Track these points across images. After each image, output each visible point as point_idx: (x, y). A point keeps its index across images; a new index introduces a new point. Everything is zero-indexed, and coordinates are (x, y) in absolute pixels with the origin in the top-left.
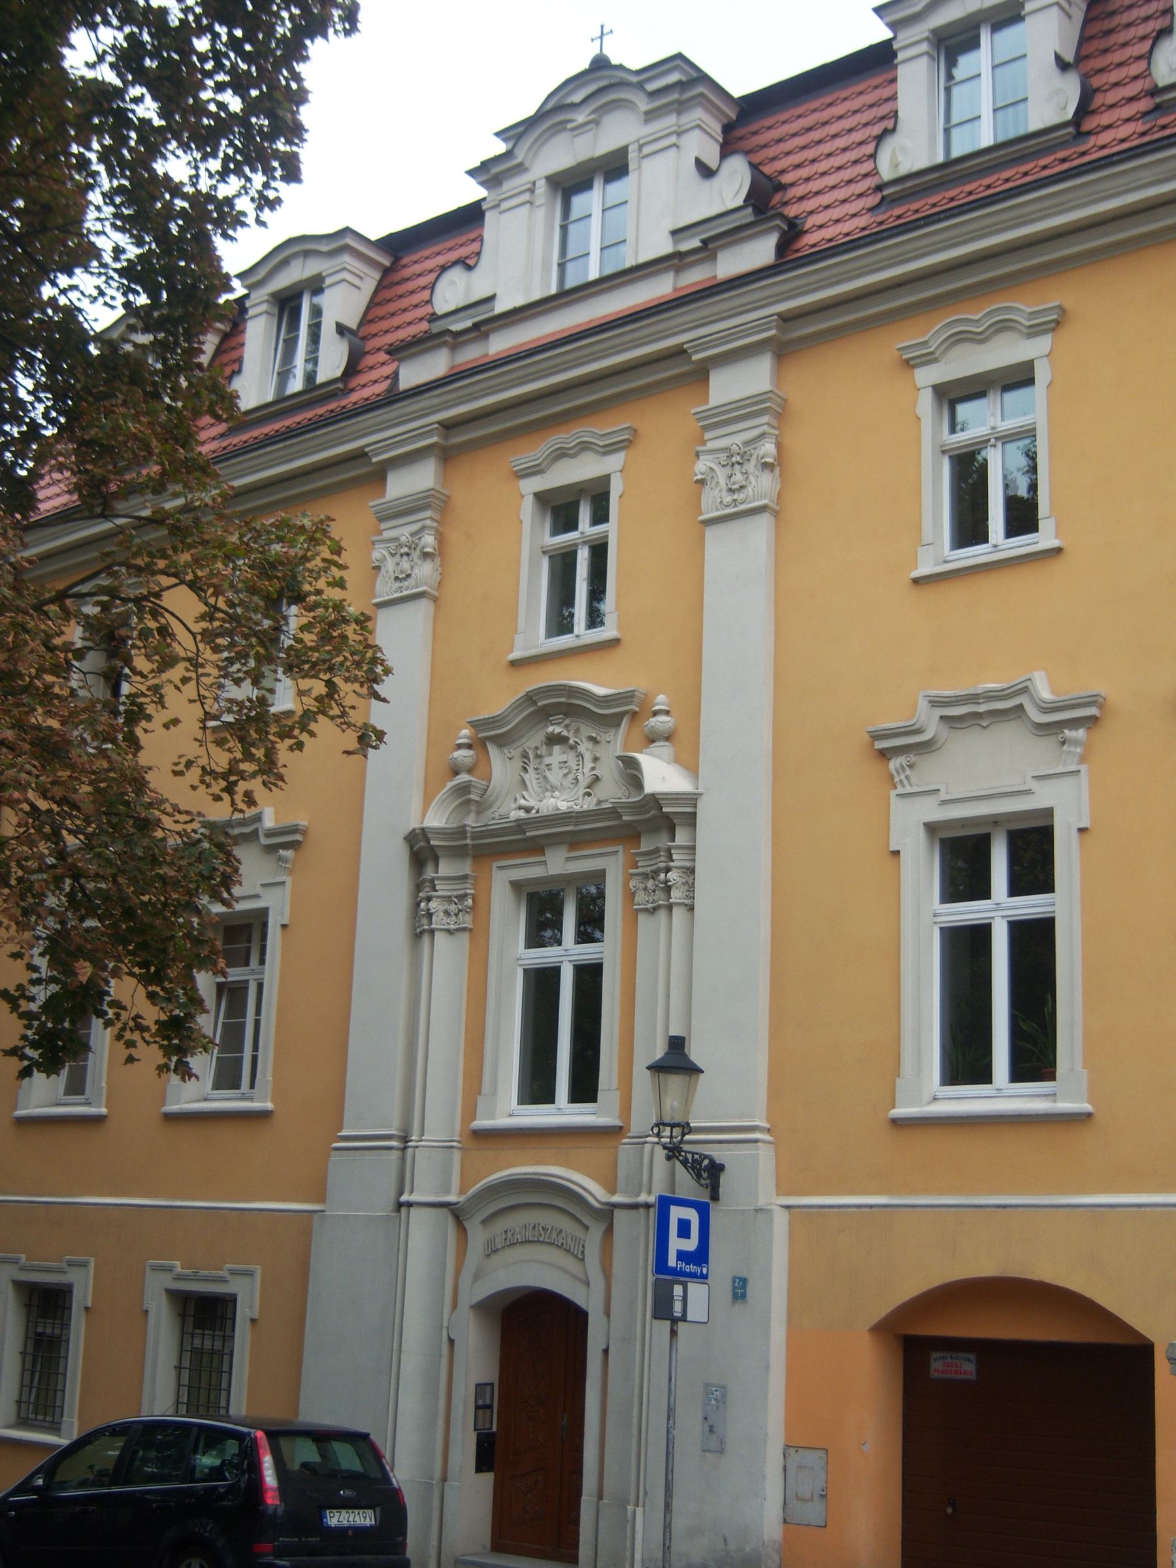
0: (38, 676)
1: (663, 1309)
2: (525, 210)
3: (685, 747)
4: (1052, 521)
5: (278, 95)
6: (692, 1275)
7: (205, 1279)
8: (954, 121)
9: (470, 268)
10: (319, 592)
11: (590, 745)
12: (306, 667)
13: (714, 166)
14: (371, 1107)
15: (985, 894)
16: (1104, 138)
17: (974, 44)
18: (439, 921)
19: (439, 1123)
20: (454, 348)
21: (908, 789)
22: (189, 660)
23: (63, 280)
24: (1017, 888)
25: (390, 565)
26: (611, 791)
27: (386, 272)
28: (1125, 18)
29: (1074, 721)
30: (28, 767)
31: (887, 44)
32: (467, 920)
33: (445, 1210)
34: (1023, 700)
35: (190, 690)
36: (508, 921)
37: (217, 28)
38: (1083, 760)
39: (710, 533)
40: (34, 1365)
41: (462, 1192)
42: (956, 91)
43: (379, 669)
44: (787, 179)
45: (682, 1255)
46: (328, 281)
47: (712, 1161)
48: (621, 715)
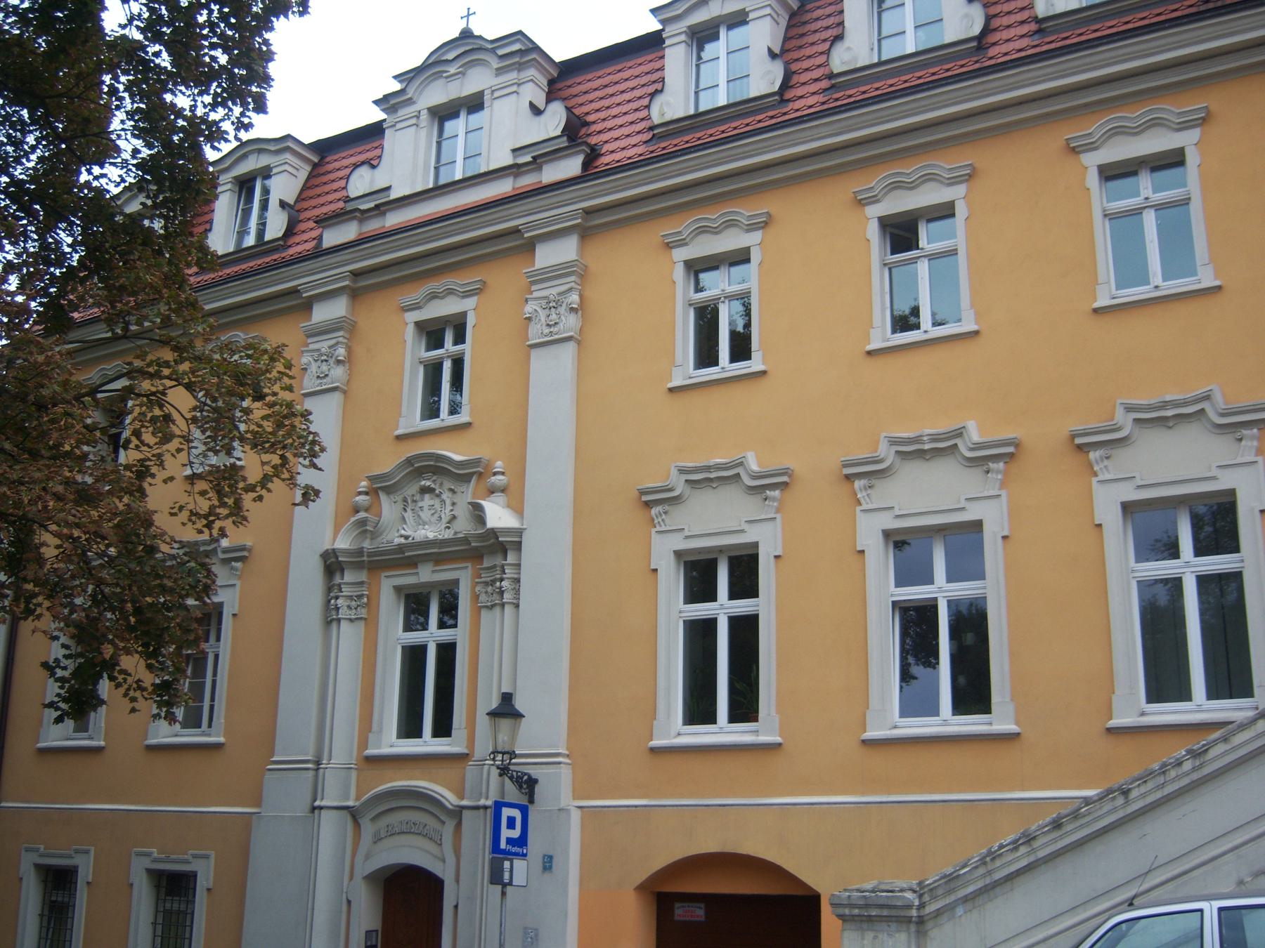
0: (78, 447)
1: (496, 877)
3: (516, 500)
5: (254, 55)
6: (516, 854)
8: (702, 87)
9: (374, 167)
10: (275, 394)
11: (450, 494)
12: (267, 445)
13: (541, 107)
14: (294, 740)
16: (798, 104)
17: (715, 37)
18: (344, 613)
19: (342, 751)
20: (361, 221)
21: (663, 528)
22: (183, 437)
23: (96, 170)
24: (733, 595)
25: (314, 367)
26: (464, 526)
27: (315, 166)
28: (813, 26)
29: (771, 485)
30: (73, 512)
32: (363, 613)
33: (344, 812)
34: (739, 470)
35: (183, 457)
36: (391, 613)
37: (213, 6)
38: (778, 511)
39: (535, 353)
40: (49, 923)
41: (357, 799)
42: (703, 67)
43: (317, 448)
44: (590, 118)
47: (530, 777)
48: (472, 474)
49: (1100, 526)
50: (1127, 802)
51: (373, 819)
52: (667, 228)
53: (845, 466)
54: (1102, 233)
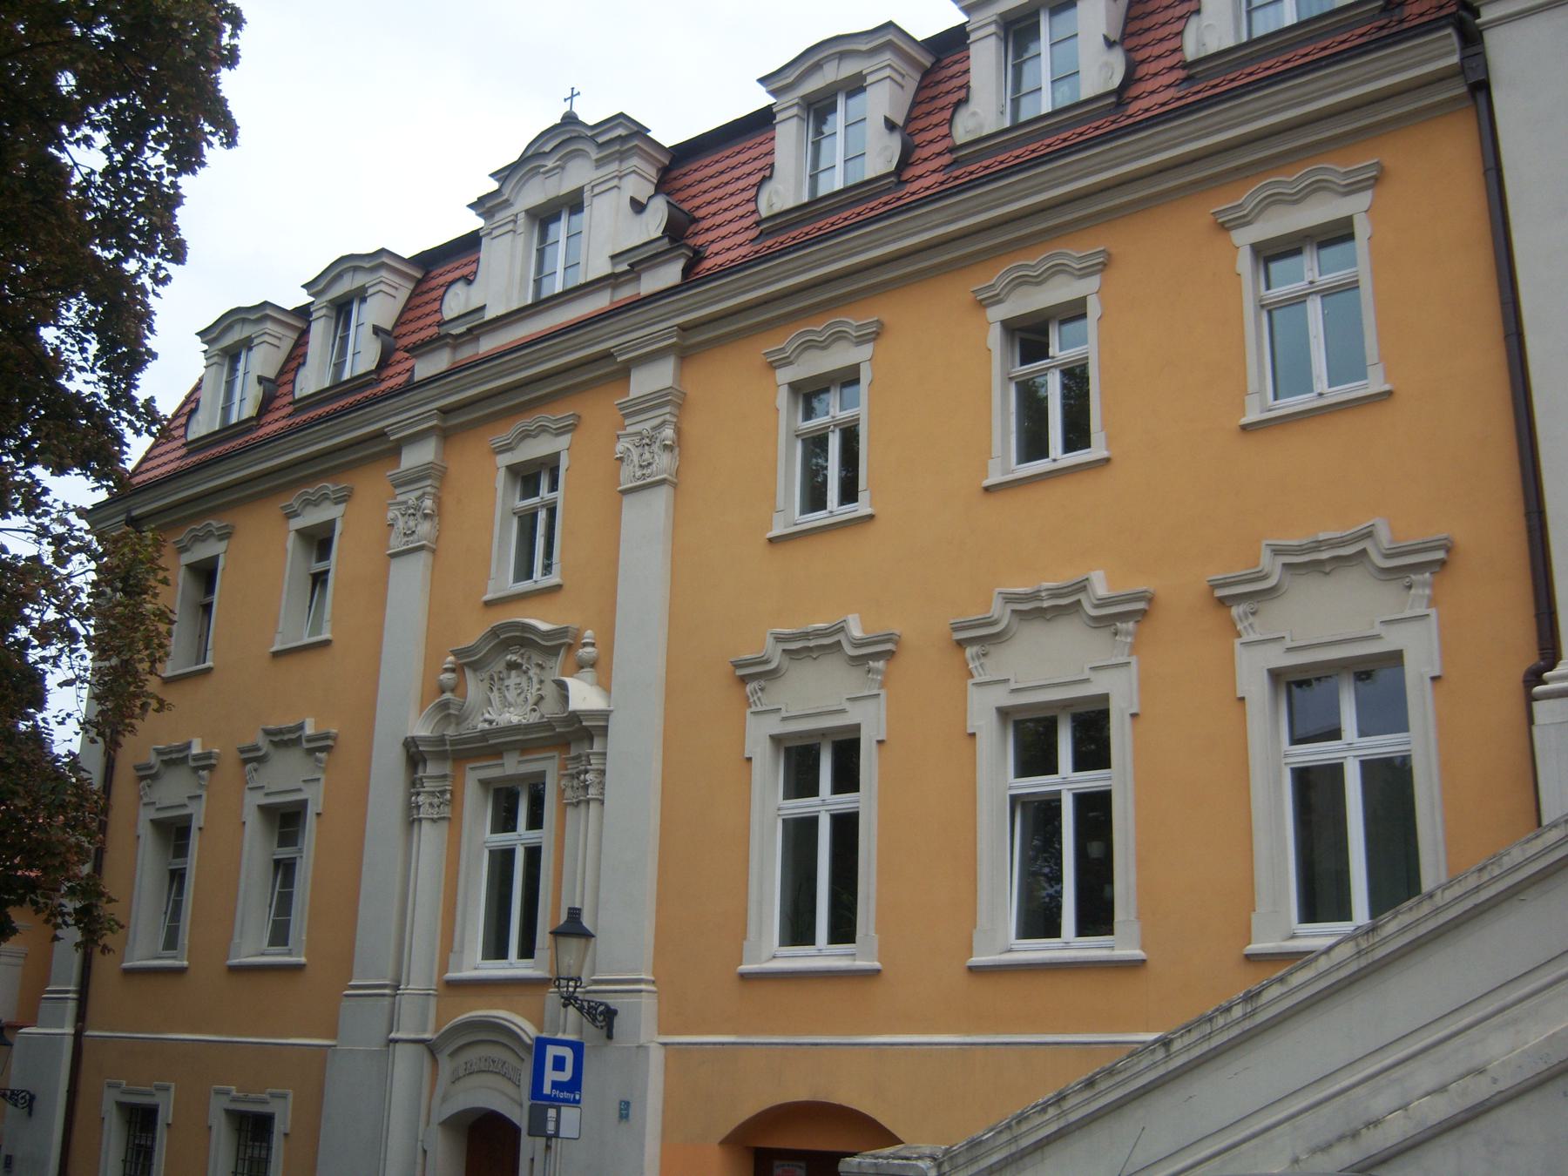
2: (509, 236)
3: (599, 669)
4: (1103, 434)
7: (254, 1101)
15: (1052, 769)
19: (420, 978)
20: (455, 348)
21: (760, 708)
25: (401, 524)
26: (550, 709)
27: (419, 282)
29: (878, 654)
31: (962, 27)
32: (446, 811)
33: (421, 1047)
34: (840, 637)
36: (477, 813)
38: (882, 685)
39: (626, 500)
41: (436, 1031)
45: (555, 1085)
46: (870, 80)
47: (607, 1006)
48: (561, 645)
49: (1242, 699)
50: (1168, 1056)
51: (453, 1054)
52: (1222, 203)
53: (956, 629)
54: (1254, 329)
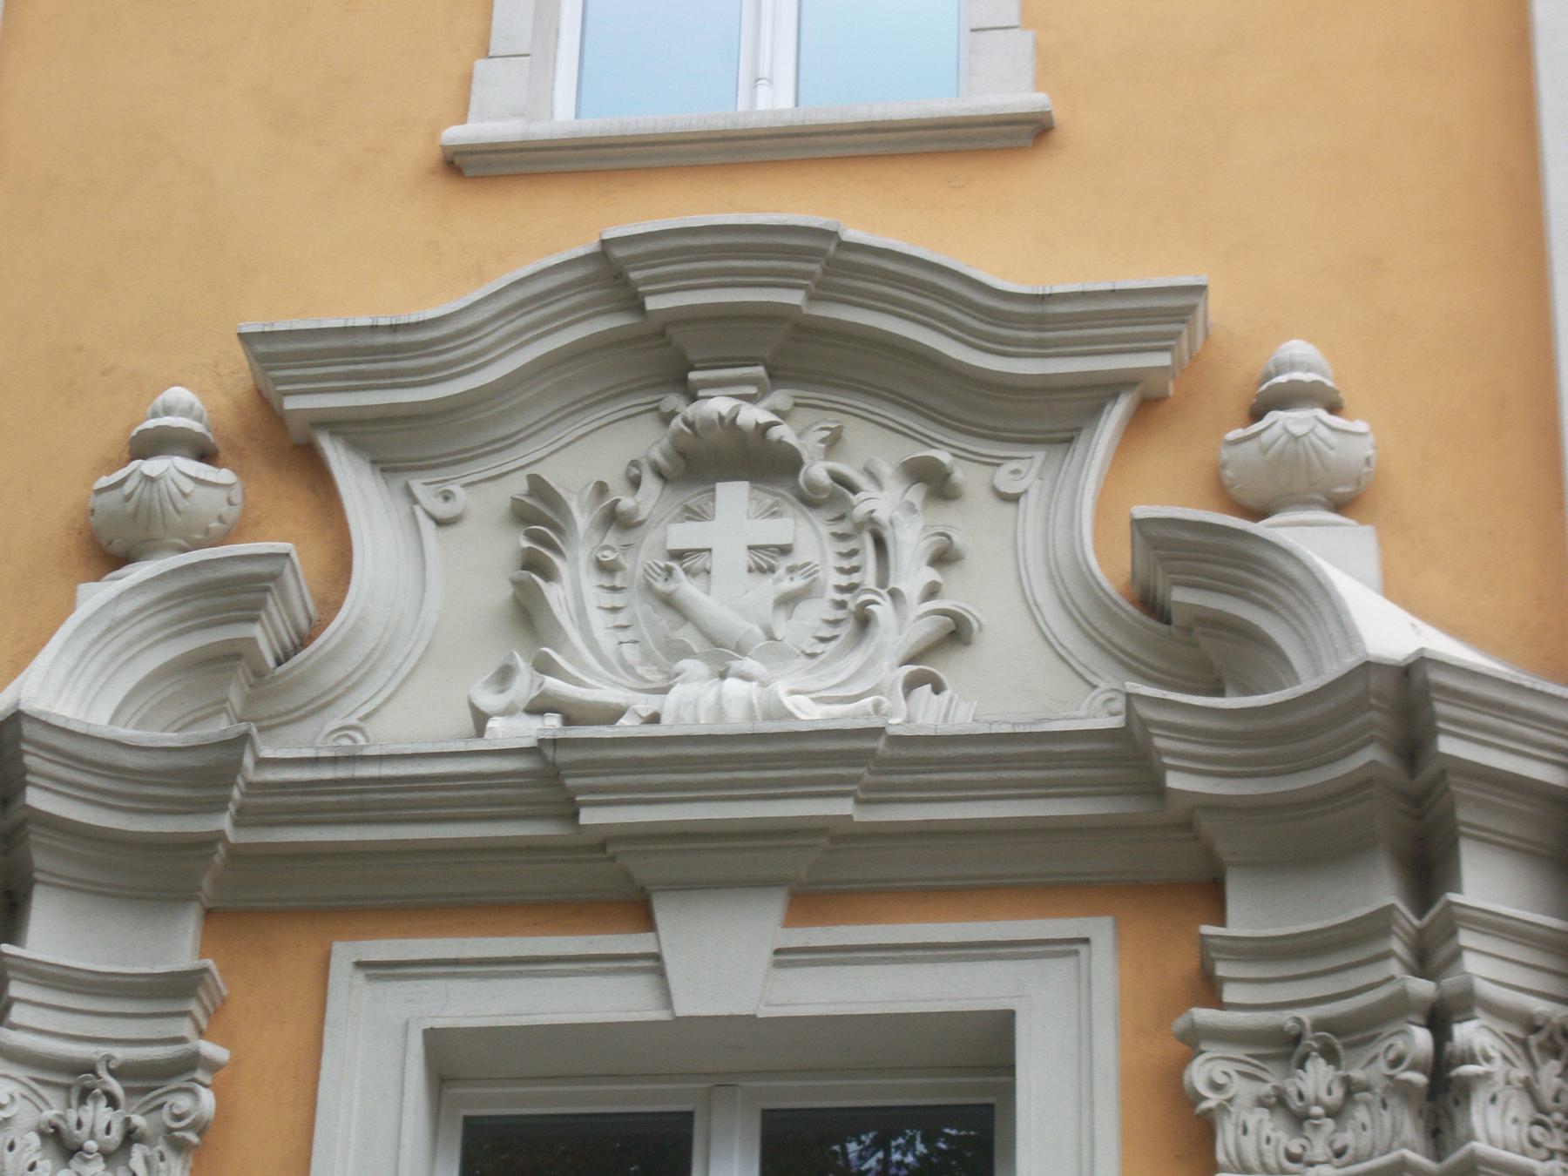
48: (1100, 392)
